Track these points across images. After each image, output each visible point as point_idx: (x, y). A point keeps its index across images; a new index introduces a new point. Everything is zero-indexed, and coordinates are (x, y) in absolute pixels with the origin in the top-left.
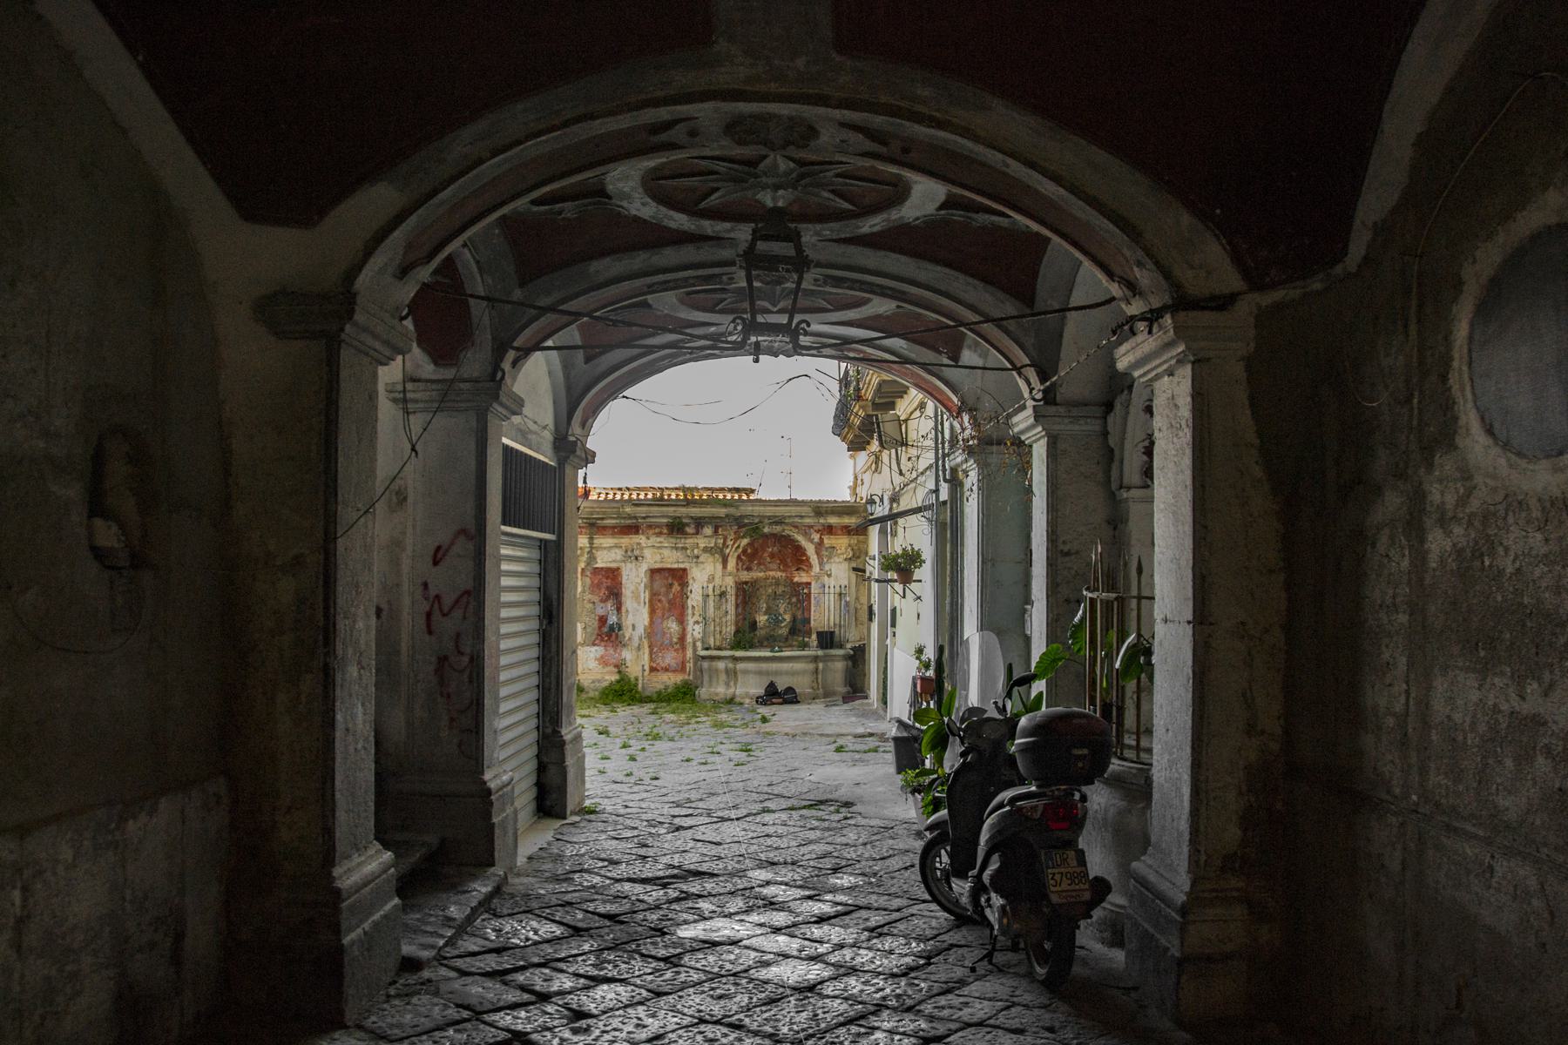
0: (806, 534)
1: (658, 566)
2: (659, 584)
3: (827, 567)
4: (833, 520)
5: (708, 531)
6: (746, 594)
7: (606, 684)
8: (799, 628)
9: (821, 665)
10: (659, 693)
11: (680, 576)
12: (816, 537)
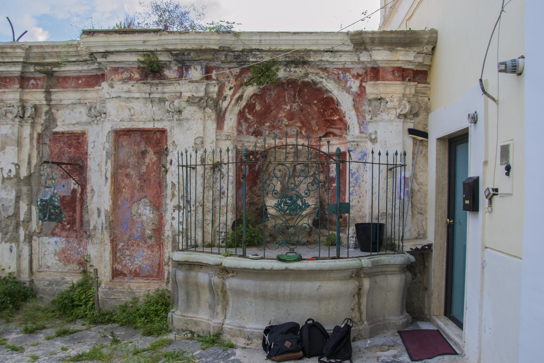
0: (338, 80)
1: (127, 125)
2: (128, 150)
3: (371, 128)
4: (381, 56)
5: (196, 73)
6: (252, 170)
7: (65, 287)
8: (329, 218)
9: (366, 283)
10: (124, 309)
11: (154, 140)
12: (355, 85)
